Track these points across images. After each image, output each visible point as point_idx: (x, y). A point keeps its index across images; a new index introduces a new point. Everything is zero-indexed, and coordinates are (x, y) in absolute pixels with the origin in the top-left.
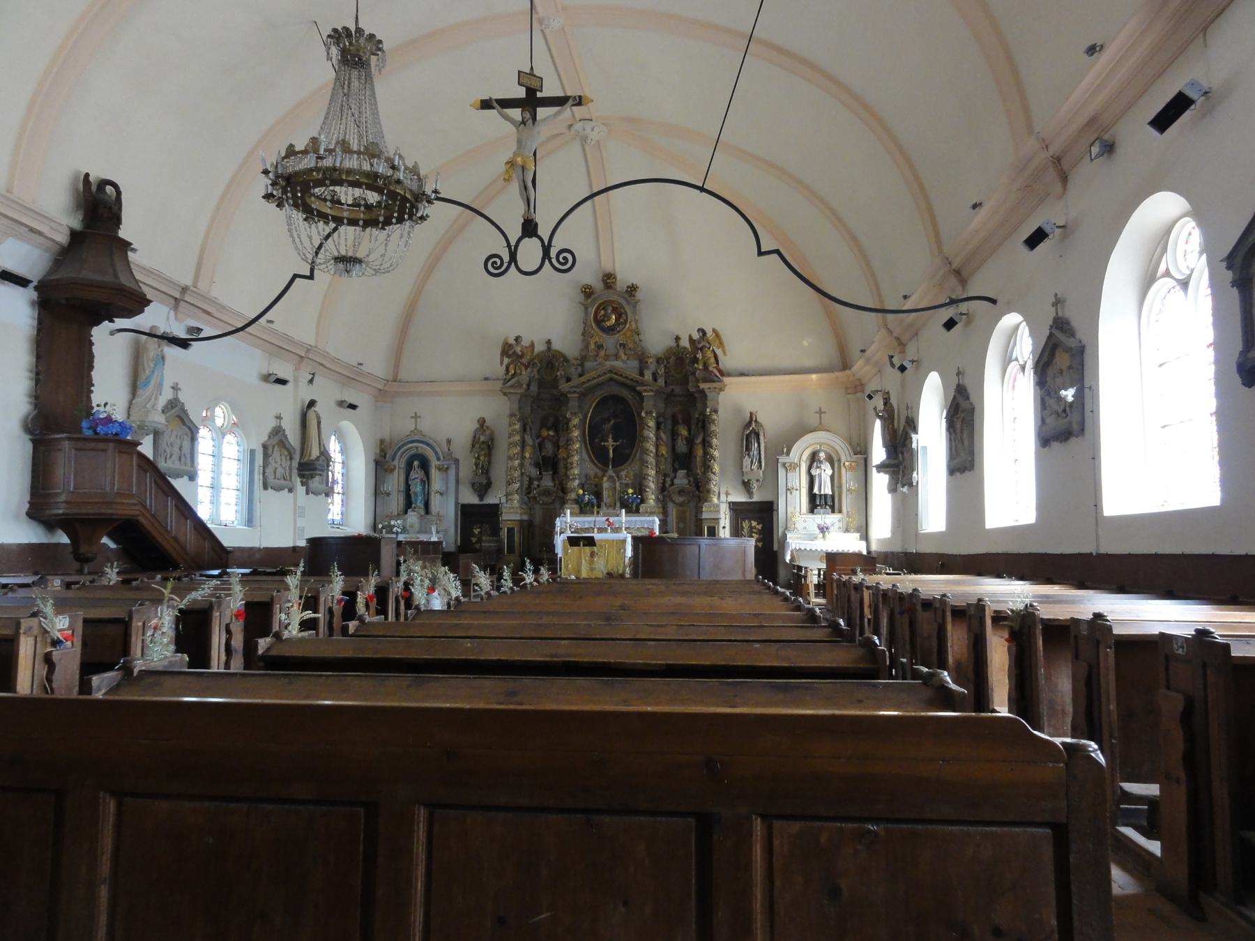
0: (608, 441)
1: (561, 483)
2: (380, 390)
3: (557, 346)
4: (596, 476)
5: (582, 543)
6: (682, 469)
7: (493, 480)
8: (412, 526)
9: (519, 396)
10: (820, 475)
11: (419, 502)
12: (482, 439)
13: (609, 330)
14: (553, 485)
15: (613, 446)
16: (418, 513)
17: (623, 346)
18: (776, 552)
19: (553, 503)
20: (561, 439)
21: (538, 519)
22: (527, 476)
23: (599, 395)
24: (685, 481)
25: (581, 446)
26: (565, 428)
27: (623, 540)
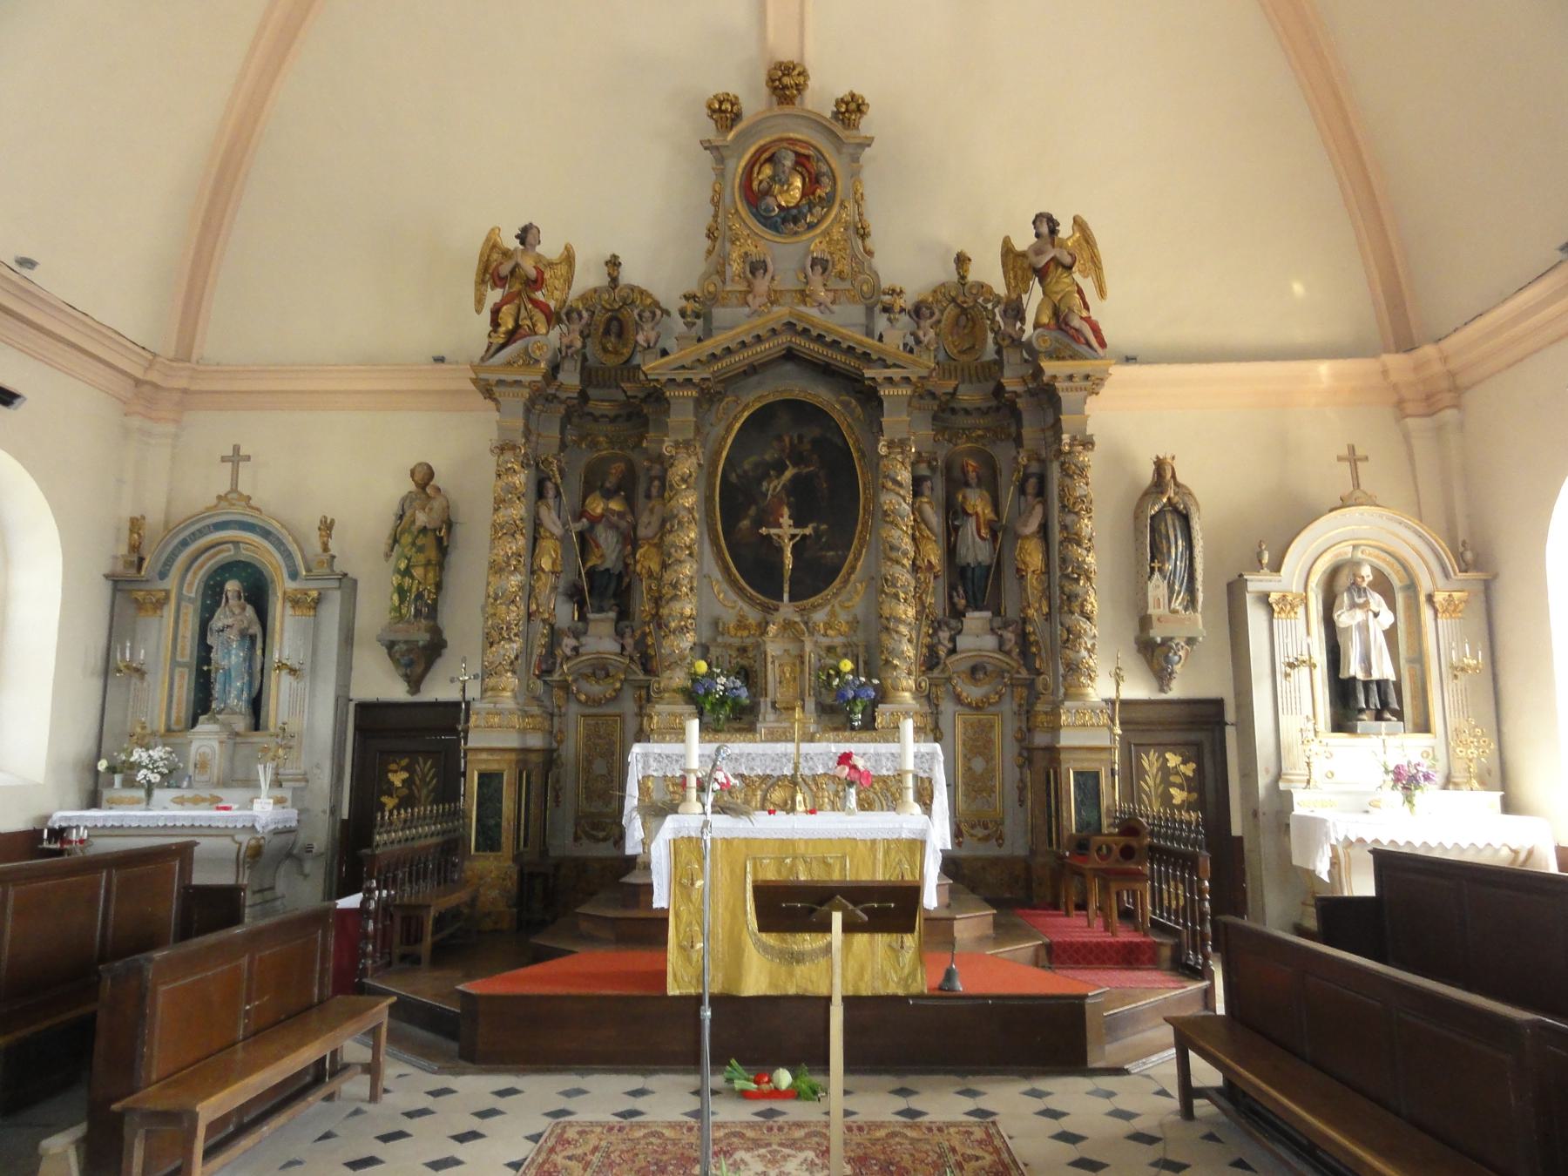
0: (780, 526)
1: (641, 644)
2: (138, 382)
3: (631, 275)
4: (742, 624)
5: (837, 918)
6: (977, 608)
7: (447, 635)
8: (202, 765)
9: (526, 393)
10: (1364, 628)
11: (232, 695)
12: (421, 519)
13: (784, 221)
14: (617, 649)
15: (793, 536)
16: (226, 726)
17: (821, 264)
18: (1240, 839)
19: (616, 698)
20: (644, 519)
21: (572, 746)
22: (544, 621)
23: (754, 398)
24: (990, 642)
25: (701, 534)
26: (654, 491)
27: (913, 841)
